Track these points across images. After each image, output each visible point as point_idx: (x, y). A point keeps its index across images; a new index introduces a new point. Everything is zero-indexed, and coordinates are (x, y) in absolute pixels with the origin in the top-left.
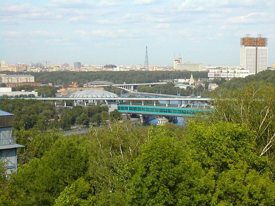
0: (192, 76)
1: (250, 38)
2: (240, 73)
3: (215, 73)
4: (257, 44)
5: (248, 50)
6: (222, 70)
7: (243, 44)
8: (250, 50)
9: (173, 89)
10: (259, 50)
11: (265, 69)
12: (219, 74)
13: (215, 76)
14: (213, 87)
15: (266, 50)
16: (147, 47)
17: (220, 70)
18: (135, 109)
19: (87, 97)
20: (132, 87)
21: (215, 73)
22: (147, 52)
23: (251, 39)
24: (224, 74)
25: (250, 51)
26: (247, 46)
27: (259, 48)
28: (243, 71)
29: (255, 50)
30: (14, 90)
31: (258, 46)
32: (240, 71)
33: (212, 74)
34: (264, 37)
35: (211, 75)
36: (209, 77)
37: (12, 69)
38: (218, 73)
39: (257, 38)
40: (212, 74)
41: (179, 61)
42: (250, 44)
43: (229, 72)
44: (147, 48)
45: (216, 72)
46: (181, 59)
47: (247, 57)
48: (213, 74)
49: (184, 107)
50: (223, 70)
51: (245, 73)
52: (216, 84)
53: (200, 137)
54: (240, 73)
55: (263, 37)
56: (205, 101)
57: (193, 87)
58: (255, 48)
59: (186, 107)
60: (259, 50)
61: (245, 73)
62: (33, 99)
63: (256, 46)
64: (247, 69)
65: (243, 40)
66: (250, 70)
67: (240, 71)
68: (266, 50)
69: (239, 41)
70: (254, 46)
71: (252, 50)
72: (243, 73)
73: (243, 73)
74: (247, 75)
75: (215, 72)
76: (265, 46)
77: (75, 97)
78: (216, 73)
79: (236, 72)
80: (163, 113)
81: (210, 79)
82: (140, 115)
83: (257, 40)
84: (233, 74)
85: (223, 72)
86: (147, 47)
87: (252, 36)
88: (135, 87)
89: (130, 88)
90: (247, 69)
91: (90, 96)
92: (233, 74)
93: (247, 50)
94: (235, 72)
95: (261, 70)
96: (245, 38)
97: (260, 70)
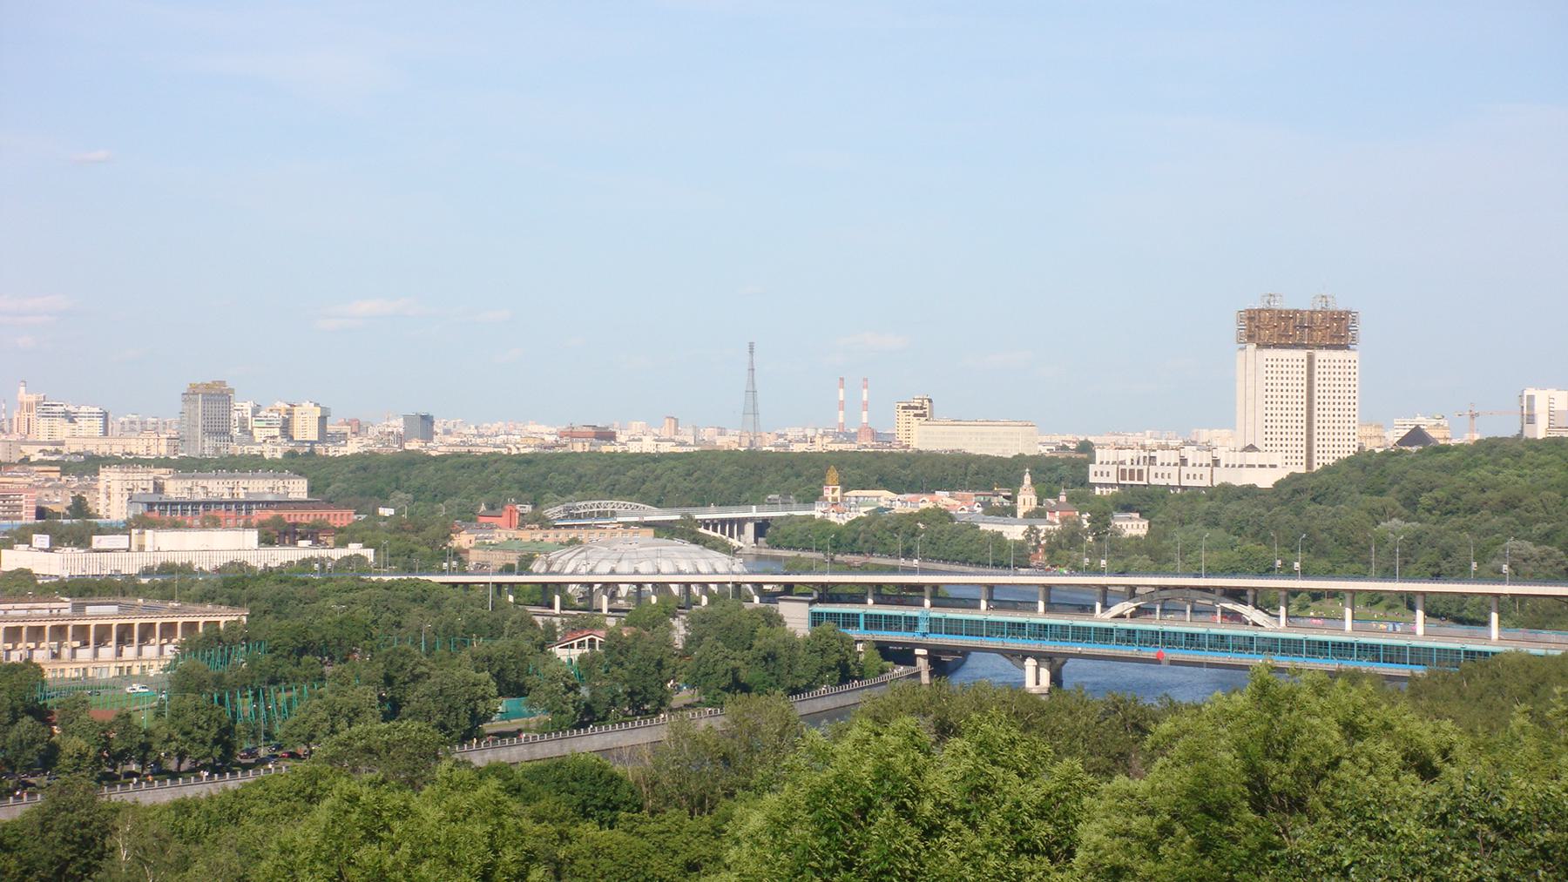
0: (1027, 479)
1: (1280, 312)
2: (1241, 466)
3: (1121, 467)
4: (1311, 337)
5: (1274, 363)
6: (1153, 454)
7: (1251, 338)
8: (1280, 363)
9: (946, 537)
10: (1322, 364)
11: (1347, 451)
12: (1140, 472)
13: (1123, 478)
14: (1133, 527)
15: (1352, 364)
16: (751, 346)
17: (1146, 454)
18: (891, 623)
19: (613, 572)
20: (750, 528)
21: (1121, 467)
22: (753, 370)
23: (1286, 317)
24: (1166, 470)
25: (1280, 369)
26: (1267, 346)
27: (1320, 355)
28: (1252, 458)
29: (1305, 364)
30: (266, 540)
31: (1320, 347)
32: (1238, 458)
33: (1106, 469)
34: (1341, 307)
35: (1103, 473)
36: (1093, 486)
37: (217, 449)
38: (1136, 468)
39: (1312, 312)
40: (1106, 469)
41: (921, 412)
42: (1280, 336)
43: (1190, 463)
44: (751, 352)
45: (1128, 462)
46: (930, 401)
47: (1269, 393)
48: (1113, 469)
49: (1124, 617)
50: (1158, 454)
51: (1261, 466)
52: (1137, 515)
53: (106, 832)
54: (1241, 466)
55: (1339, 305)
56: (1221, 588)
57: (1039, 527)
58: (1302, 354)
59: (1133, 615)
60: (1322, 364)
61: (1261, 466)
62: (421, 578)
63: (1305, 347)
64: (1269, 448)
65: (1251, 319)
66: (1289, 454)
67: (1238, 458)
68: (1352, 364)
69: (1230, 327)
70: (1295, 346)
71: (1342, 364)
72: (1254, 466)
73: (1254, 466)
74: (1281, 474)
75: (1123, 463)
76: (1348, 348)
77: (555, 568)
78: (1128, 467)
79: (1222, 464)
80: (964, 637)
81: (1098, 491)
82: (918, 651)
83: (1312, 320)
84: (1209, 469)
85: (1158, 463)
86: (751, 346)
87: (1286, 304)
88: (762, 528)
89: (741, 531)
90: (1269, 448)
91: (624, 567)
92: (1209, 469)
93: (1270, 363)
94: (1216, 462)
95: (1336, 455)
96: (1260, 311)
97: (1326, 456)
